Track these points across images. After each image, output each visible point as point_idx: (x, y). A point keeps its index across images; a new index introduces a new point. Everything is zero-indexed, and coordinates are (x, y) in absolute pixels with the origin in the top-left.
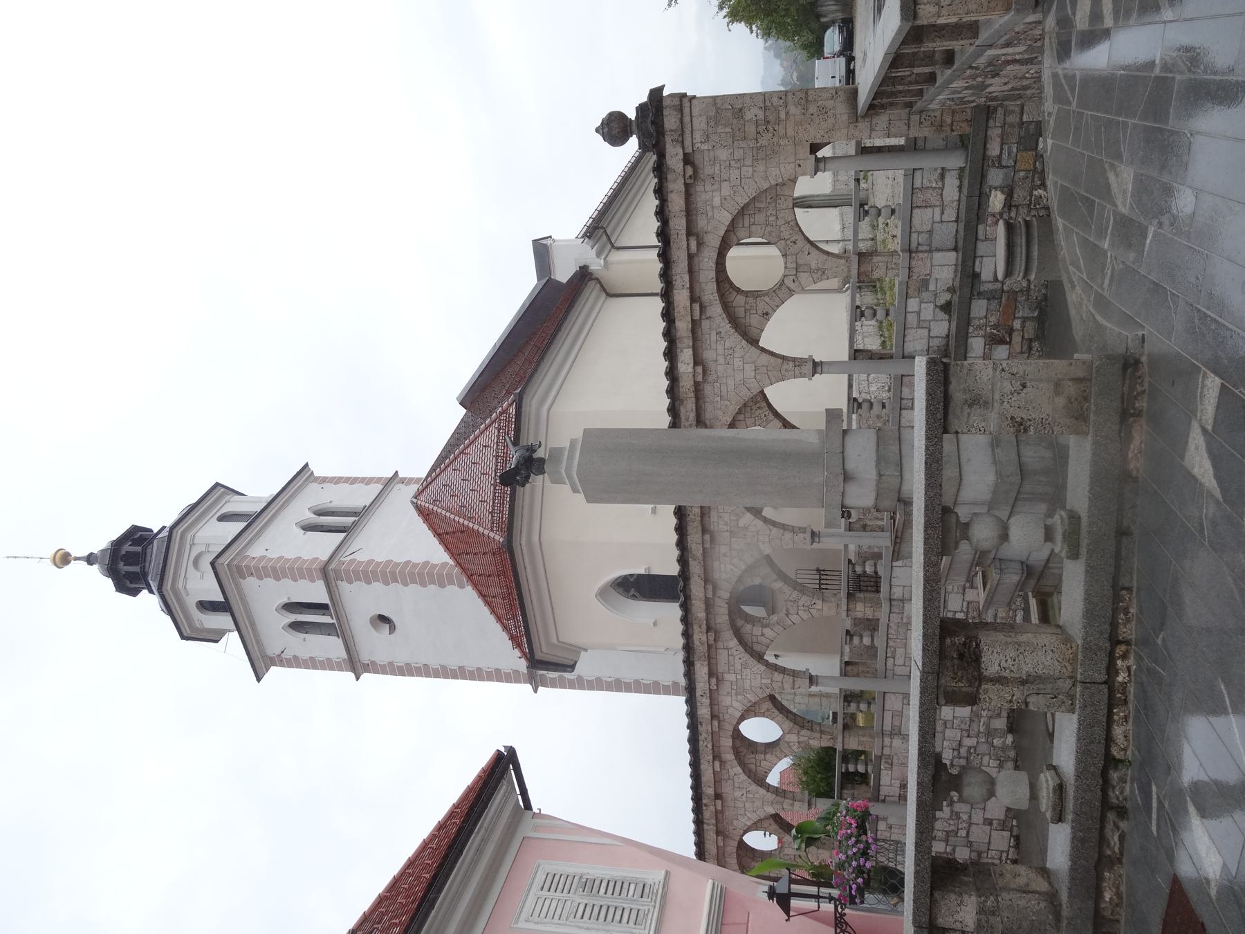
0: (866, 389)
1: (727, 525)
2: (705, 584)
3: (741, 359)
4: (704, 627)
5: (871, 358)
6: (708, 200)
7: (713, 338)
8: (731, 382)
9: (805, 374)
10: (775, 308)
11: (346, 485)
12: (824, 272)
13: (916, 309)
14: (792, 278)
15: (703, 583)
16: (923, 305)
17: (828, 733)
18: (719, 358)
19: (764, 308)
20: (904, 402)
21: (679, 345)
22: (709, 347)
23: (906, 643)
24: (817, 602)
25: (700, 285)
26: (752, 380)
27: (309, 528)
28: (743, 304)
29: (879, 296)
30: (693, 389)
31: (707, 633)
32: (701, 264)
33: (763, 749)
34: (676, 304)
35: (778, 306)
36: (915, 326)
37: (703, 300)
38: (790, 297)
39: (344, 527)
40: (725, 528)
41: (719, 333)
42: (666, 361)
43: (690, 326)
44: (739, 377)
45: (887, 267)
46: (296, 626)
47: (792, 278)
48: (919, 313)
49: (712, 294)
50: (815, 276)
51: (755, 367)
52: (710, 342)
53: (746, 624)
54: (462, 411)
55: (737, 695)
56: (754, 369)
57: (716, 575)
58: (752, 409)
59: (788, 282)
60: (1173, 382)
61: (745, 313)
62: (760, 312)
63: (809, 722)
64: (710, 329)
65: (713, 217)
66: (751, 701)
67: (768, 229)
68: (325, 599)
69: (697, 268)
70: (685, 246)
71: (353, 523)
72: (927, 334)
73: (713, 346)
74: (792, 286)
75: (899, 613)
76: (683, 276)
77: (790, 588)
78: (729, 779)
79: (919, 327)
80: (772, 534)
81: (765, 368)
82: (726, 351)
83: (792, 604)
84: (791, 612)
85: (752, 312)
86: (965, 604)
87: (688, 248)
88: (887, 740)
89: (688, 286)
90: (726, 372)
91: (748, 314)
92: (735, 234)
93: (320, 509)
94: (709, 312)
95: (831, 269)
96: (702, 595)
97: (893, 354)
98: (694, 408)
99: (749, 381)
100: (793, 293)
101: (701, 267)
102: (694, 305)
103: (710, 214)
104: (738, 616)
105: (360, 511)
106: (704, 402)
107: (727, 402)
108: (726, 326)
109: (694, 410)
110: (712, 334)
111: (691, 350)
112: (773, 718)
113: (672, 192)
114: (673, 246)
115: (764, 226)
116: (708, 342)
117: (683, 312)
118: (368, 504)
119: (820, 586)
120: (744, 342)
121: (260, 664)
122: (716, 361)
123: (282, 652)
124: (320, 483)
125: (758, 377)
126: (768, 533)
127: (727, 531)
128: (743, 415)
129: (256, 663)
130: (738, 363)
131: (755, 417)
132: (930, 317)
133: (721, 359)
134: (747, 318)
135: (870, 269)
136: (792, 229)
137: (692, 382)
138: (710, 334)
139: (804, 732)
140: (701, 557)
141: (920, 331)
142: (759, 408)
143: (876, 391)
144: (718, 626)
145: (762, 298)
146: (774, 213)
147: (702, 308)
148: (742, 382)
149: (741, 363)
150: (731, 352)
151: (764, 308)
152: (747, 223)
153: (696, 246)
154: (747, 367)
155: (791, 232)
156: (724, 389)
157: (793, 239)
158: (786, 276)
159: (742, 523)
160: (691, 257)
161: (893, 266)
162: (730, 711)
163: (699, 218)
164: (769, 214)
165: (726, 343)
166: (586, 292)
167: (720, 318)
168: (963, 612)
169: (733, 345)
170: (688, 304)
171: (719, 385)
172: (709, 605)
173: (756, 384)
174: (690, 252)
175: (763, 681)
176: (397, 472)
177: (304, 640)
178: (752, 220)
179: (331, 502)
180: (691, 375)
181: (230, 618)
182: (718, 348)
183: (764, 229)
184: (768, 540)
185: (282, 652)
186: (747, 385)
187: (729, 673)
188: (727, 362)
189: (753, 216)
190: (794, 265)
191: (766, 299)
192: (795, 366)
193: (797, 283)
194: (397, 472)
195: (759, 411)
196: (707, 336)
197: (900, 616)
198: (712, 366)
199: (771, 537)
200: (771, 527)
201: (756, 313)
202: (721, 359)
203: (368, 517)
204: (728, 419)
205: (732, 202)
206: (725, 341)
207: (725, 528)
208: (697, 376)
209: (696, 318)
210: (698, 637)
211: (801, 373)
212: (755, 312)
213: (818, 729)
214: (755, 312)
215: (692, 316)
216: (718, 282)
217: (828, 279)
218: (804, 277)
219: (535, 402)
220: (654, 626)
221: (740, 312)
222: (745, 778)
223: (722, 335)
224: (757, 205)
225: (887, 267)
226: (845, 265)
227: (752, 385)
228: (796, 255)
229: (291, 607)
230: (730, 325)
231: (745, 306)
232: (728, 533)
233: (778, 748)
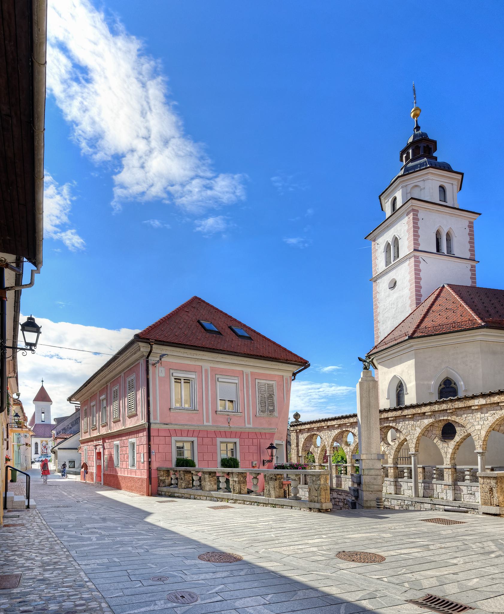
11: (468, 239)
20: (470, 488)
43: (496, 402)
60: (99, 353)
66: (148, 352)
96: (389, 416)
98: (460, 407)
99: (474, 428)
109: (459, 407)
111: (485, 403)
120: (490, 424)
137: (471, 405)
139: (351, 453)
140: (402, 414)
149: (481, 424)
180: (473, 404)
181: (390, 214)
195: (463, 432)
196: (493, 409)
222: (334, 435)
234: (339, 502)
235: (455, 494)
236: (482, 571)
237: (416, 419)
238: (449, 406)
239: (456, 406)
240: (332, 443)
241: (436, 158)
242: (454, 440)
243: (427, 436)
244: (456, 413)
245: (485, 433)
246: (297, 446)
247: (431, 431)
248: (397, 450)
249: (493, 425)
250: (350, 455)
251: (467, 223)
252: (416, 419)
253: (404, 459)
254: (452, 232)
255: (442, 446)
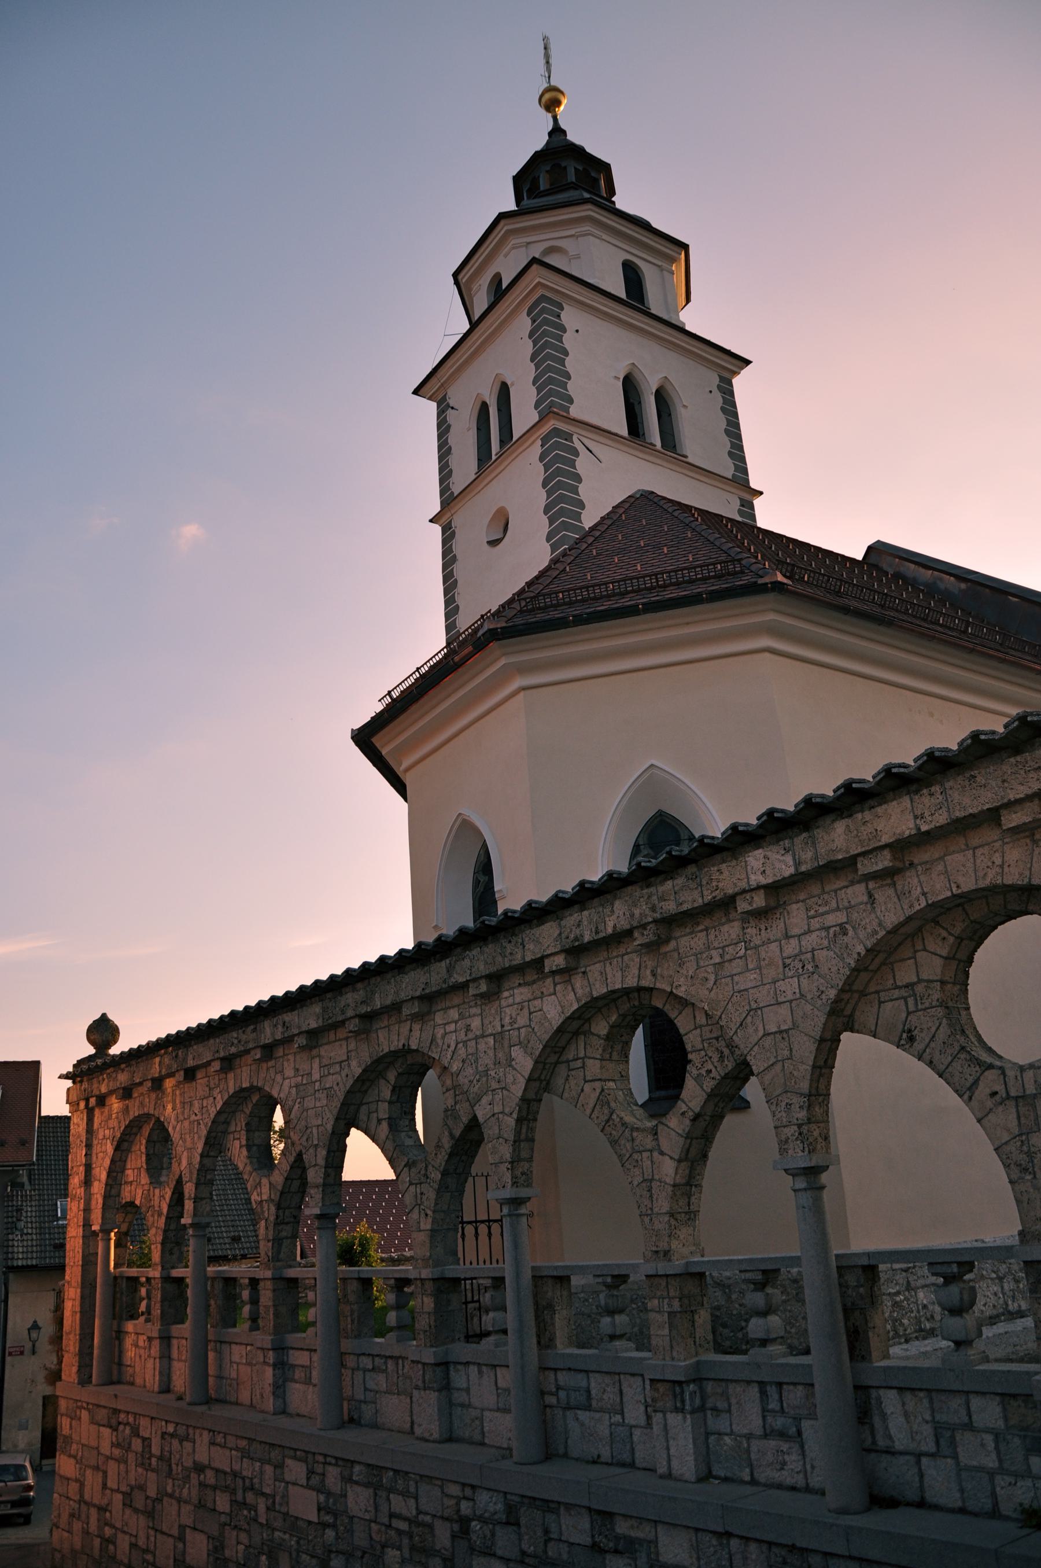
0: (921, 1282)
2: (418, 997)
3: (798, 995)
4: (364, 1009)
5: (847, 1311)
9: (786, 1150)
11: (723, 424)
12: (1026, 1170)
13: (978, 1420)
14: (999, 1087)
15: (418, 994)
16: (989, 1439)
17: (279, 1252)
18: (794, 942)
19: (922, 1030)
21: (799, 840)
22: (812, 913)
24: (430, 1220)
26: (761, 1028)
27: (630, 386)
28: (924, 976)
30: (719, 895)
31: (356, 1016)
32: (986, 850)
34: (880, 810)
35: (930, 1064)
36: (938, 1417)
37: (908, 874)
38: (956, 1091)
39: (644, 434)
42: (759, 819)
44: (763, 996)
47: (999, 1087)
48: (969, 1426)
49: (924, 894)
51: (787, 1031)
52: (822, 914)
53: (391, 1088)
54: (858, 554)
55: (297, 1086)
56: (783, 1028)
58: (717, 1039)
59: (990, 1081)
61: (906, 986)
63: (295, 1217)
64: (850, 907)
69: (975, 841)
70: (1012, 796)
72: (924, 1448)
73: (815, 923)
74: (982, 1092)
75: (424, 1382)
77: (443, 1164)
79: (938, 1430)
80: (505, 1117)
82: (809, 955)
83: (423, 1172)
84: (413, 1170)
85: (911, 1001)
86: (428, 1519)
87: (1010, 805)
89: (924, 828)
91: (903, 993)
93: (669, 394)
94: (884, 895)
97: (870, 1361)
102: (887, 853)
104: (400, 1071)
105: (678, 452)
106: (706, 929)
112: (285, 1155)
114: (1008, 765)
116: (822, 910)
117: (866, 831)
118: (690, 460)
119: (482, 1222)
120: (832, 993)
121: (434, 385)
122: (787, 937)
123: (452, 408)
125: (768, 1041)
126: (507, 1110)
127: (503, 1026)
128: (704, 1021)
129: (433, 380)
130: (789, 987)
131: (703, 1049)
132: (964, 1459)
133: (791, 947)
134: (896, 993)
137: (730, 891)
138: (838, 909)
141: (928, 1430)
142: (722, 1057)
143: (916, 1303)
144: (374, 1035)
145: (944, 1021)
147: (888, 875)
148: (754, 1006)
150: (810, 967)
151: (922, 1030)
153: (1021, 822)
154: (784, 1011)
156: (736, 966)
158: (1004, 1073)
159: (516, 1052)
160: (993, 816)
165: (825, 952)
167: (875, 923)
168: (418, 1514)
169: (823, 970)
170: (885, 839)
173: (754, 1039)
174: (1003, 812)
175: (315, 1130)
176: (761, 493)
177: (469, 430)
179: (685, 406)
180: (743, 885)
182: (814, 935)
184: (496, 1111)
185: (452, 408)
186: (749, 1018)
187: (320, 1067)
188: (788, 961)
191: (944, 1032)
192: (800, 1126)
193: (989, 1104)
194: (761, 493)
195: (715, 1057)
196: (834, 904)
197: (420, 1383)
198: (777, 929)
199: (501, 1116)
200: (515, 1116)
201: (909, 1013)
202: (791, 947)
203: (665, 464)
204: (683, 989)
206: (828, 948)
208: (745, 899)
209: (859, 866)
210: (350, 1001)
211: (786, 1141)
213: (284, 1234)
214: (911, 1008)
215: (863, 854)
216: (961, 901)
217: (1011, 1182)
218: (1007, 1118)
220: (434, 927)
227: (751, 1030)
230: (863, 953)
231: (920, 981)
232: (499, 1029)
234: (214, 1488)
235: (708, 1434)
236: (941, 579)
237: (511, 1000)
238: (637, 912)
239: (670, 907)
240: (206, 1161)
241: (614, 203)
242: (681, 1107)
243: (566, 1095)
244: (677, 950)
245: (813, 1047)
246: (87, 1182)
247: (579, 1063)
248: (135, 1130)
249: (846, 996)
250: (272, 1218)
251: (716, 381)
252: (511, 1000)
253: (483, 1229)
254: (668, 387)
255: (629, 1145)
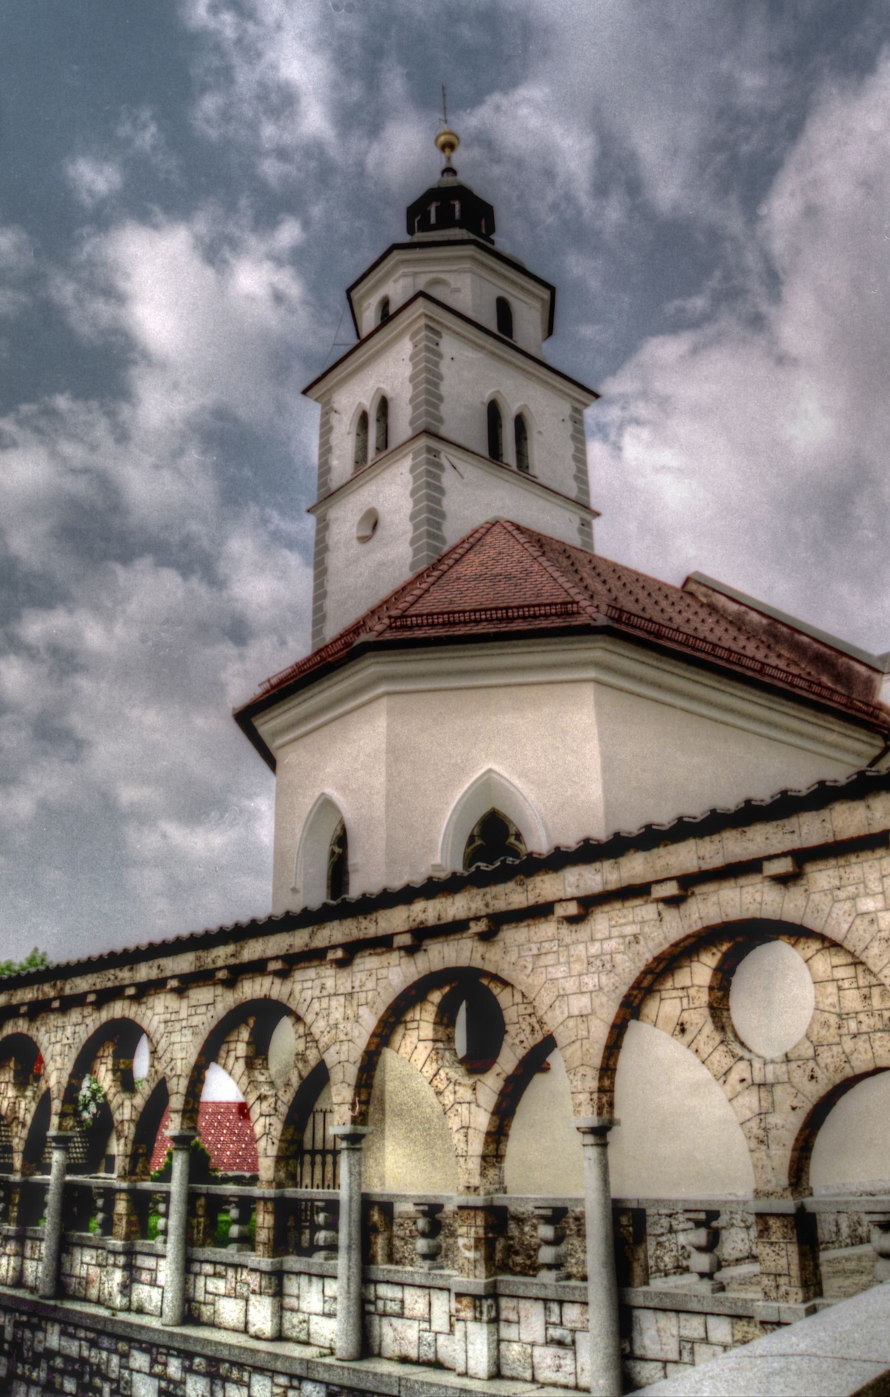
1: (360, 987)
3: (597, 988)
6: (866, 887)
7: (629, 930)
8: (559, 972)
10: (694, 1046)
12: (762, 1142)
18: (597, 945)
22: (613, 923)
23: (231, 1297)
25: (715, 891)
27: (493, 411)
29: (672, 1271)
33: (122, 1066)
40: (357, 984)
41: (636, 938)
44: (570, 985)
45: (780, 1275)
46: (364, 419)
48: (706, 1340)
49: (701, 918)
50: (754, 1124)
52: (621, 925)
57: (298, 975)
58: (530, 1015)
61: (683, 988)
62: (686, 1016)
65: (836, 901)
67: (833, 1020)
68: (393, 443)
71: (507, 464)
73: (615, 932)
74: (734, 1077)
76: (720, 855)
78: (83, 1017)
79: (682, 1340)
81: (585, 1033)
82: (608, 957)
85: (685, 1001)
87: (770, 858)
88: (121, 1260)
90: (576, 961)
91: (680, 993)
92: (818, 951)
94: (670, 915)
95: (768, 1156)
100: (721, 1081)
101: (745, 890)
103: (842, 894)
107: (530, 966)
108: (648, 952)
110: (634, 926)
113: (868, 807)
115: (837, 1010)
116: (622, 921)
124: (572, 417)
125: (571, 1023)
130: (591, 982)
133: (595, 949)
134: (674, 993)
135: (774, 1239)
136: (836, 1071)
138: (634, 922)
146: (864, 1028)
152: (841, 973)
155: (831, 1068)
156: (550, 959)
157: (818, 1073)
161: (783, 1289)
162: (149, 1013)
163: (830, 872)
164: (862, 1017)
166: (863, 735)
171: (555, 949)
172: (257, 968)
173: (560, 1019)
175: (179, 1063)
178: (846, 984)
183: (832, 1010)
188: (591, 960)
189: (854, 985)
190: (770, 1078)
193: (739, 1087)
198: (583, 931)
202: (595, 949)
205: (868, 937)
207: (357, 984)
211: (580, 1105)
212: (685, 1006)
218: (750, 1101)
219: (597, 654)
221: (682, 977)
223: (634, 945)
224: (876, 991)
225: (780, 1275)
226: (777, 1185)
227: (558, 1012)
228: (789, 1081)
229: (384, 405)
233: (120, 1089)
